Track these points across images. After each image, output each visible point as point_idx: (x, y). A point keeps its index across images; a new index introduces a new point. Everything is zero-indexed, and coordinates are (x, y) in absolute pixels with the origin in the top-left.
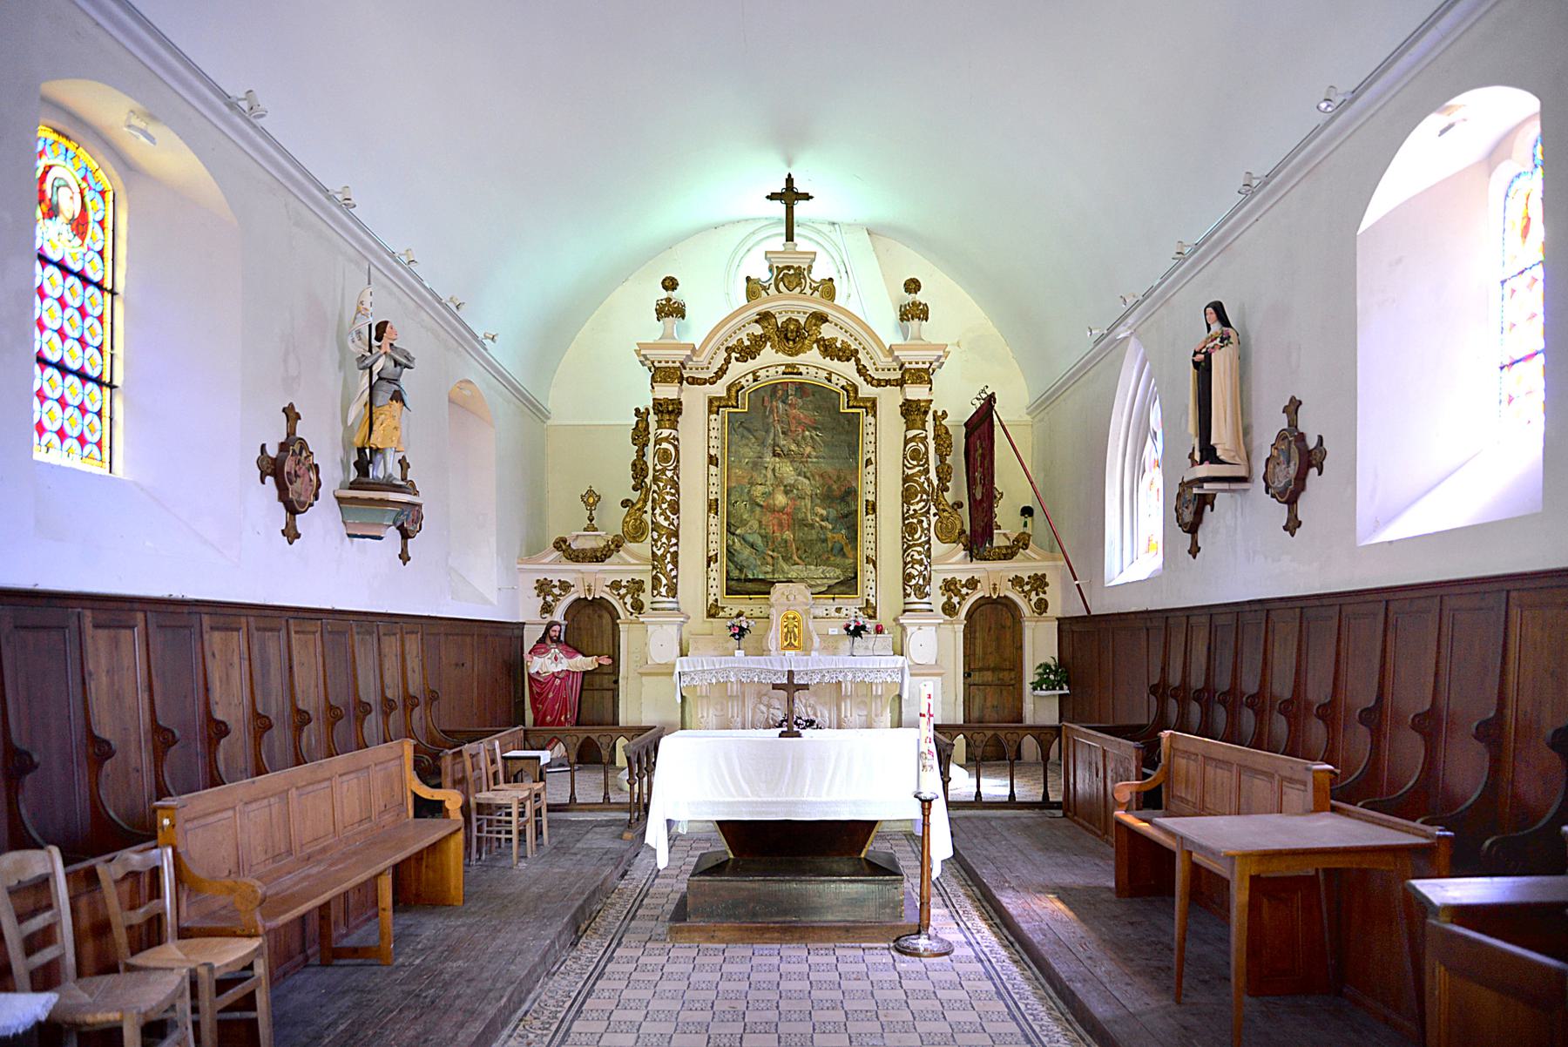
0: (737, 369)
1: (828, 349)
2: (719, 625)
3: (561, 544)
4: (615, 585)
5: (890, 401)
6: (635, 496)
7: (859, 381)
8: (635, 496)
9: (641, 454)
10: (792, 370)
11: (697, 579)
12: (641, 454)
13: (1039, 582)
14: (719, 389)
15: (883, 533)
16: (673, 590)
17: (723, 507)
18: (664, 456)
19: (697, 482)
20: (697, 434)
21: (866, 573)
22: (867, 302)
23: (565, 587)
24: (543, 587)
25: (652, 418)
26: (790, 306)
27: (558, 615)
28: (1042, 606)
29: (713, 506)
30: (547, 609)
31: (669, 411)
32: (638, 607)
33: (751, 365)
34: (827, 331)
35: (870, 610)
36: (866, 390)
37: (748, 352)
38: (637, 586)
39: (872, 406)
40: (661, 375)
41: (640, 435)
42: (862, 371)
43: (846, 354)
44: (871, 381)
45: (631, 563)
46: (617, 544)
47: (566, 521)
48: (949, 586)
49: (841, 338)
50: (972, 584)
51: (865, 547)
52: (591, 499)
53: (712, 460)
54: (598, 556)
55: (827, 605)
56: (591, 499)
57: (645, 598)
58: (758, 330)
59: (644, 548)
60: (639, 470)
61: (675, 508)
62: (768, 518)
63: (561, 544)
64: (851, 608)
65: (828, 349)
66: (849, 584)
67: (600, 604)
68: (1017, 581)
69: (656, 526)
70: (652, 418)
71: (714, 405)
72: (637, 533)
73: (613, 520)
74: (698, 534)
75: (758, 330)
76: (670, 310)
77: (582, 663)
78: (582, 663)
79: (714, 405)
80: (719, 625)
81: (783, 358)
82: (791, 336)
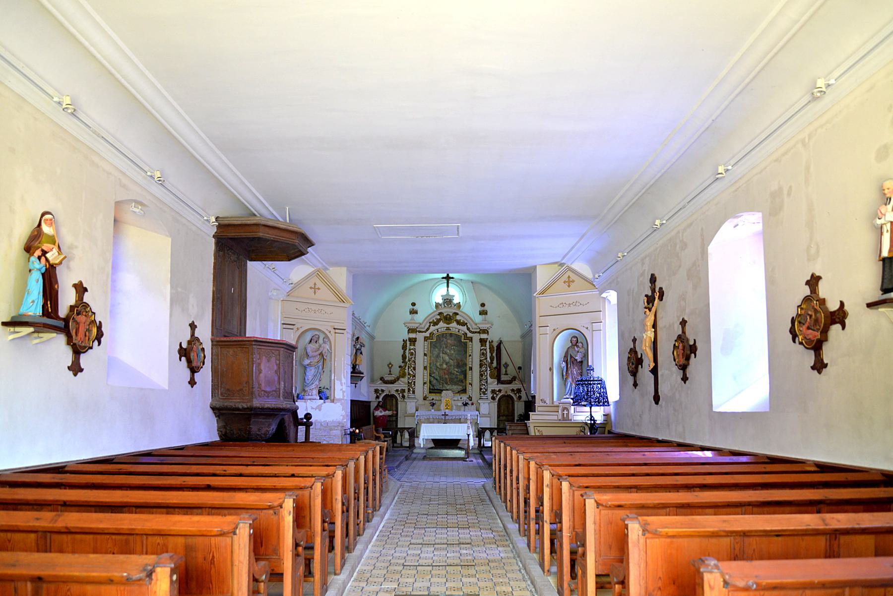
0: (432, 328)
1: (458, 322)
2: (427, 402)
3: (382, 379)
4: (397, 391)
5: (476, 338)
6: (403, 365)
7: (467, 332)
8: (403, 365)
9: (404, 352)
10: (448, 329)
11: (421, 389)
12: (404, 352)
13: (519, 391)
14: (427, 334)
15: (474, 376)
16: (414, 392)
17: (428, 369)
18: (412, 354)
19: (421, 361)
20: (421, 347)
21: (469, 388)
22: (470, 310)
23: (383, 391)
24: (376, 391)
25: (408, 343)
26: (447, 311)
27: (380, 399)
28: (520, 398)
29: (425, 368)
30: (377, 397)
31: (413, 341)
32: (403, 397)
33: (437, 327)
34: (458, 318)
35: (470, 398)
36: (469, 335)
37: (435, 324)
38: (403, 391)
39: (471, 339)
40: (411, 331)
41: (404, 347)
42: (468, 329)
43: (464, 324)
44: (471, 332)
45: (402, 384)
46: (398, 379)
47: (383, 371)
48: (493, 391)
49: (462, 320)
50: (500, 391)
51: (469, 381)
52: (390, 365)
53: (425, 355)
54: (392, 382)
55: (458, 397)
56: (390, 365)
57: (406, 394)
58: (439, 317)
59: (405, 380)
60: (404, 357)
61: (414, 369)
62: (441, 372)
63: (382, 379)
64: (465, 397)
65: (458, 322)
66: (464, 391)
67: (393, 396)
68: (513, 390)
69: (409, 374)
70: (408, 343)
71: (426, 339)
72: (403, 376)
73: (396, 371)
74: (421, 376)
75: (439, 317)
76: (413, 312)
77: (388, 413)
78: (388, 413)
79: (426, 339)
80: (427, 402)
81: (446, 325)
82: (448, 319)
